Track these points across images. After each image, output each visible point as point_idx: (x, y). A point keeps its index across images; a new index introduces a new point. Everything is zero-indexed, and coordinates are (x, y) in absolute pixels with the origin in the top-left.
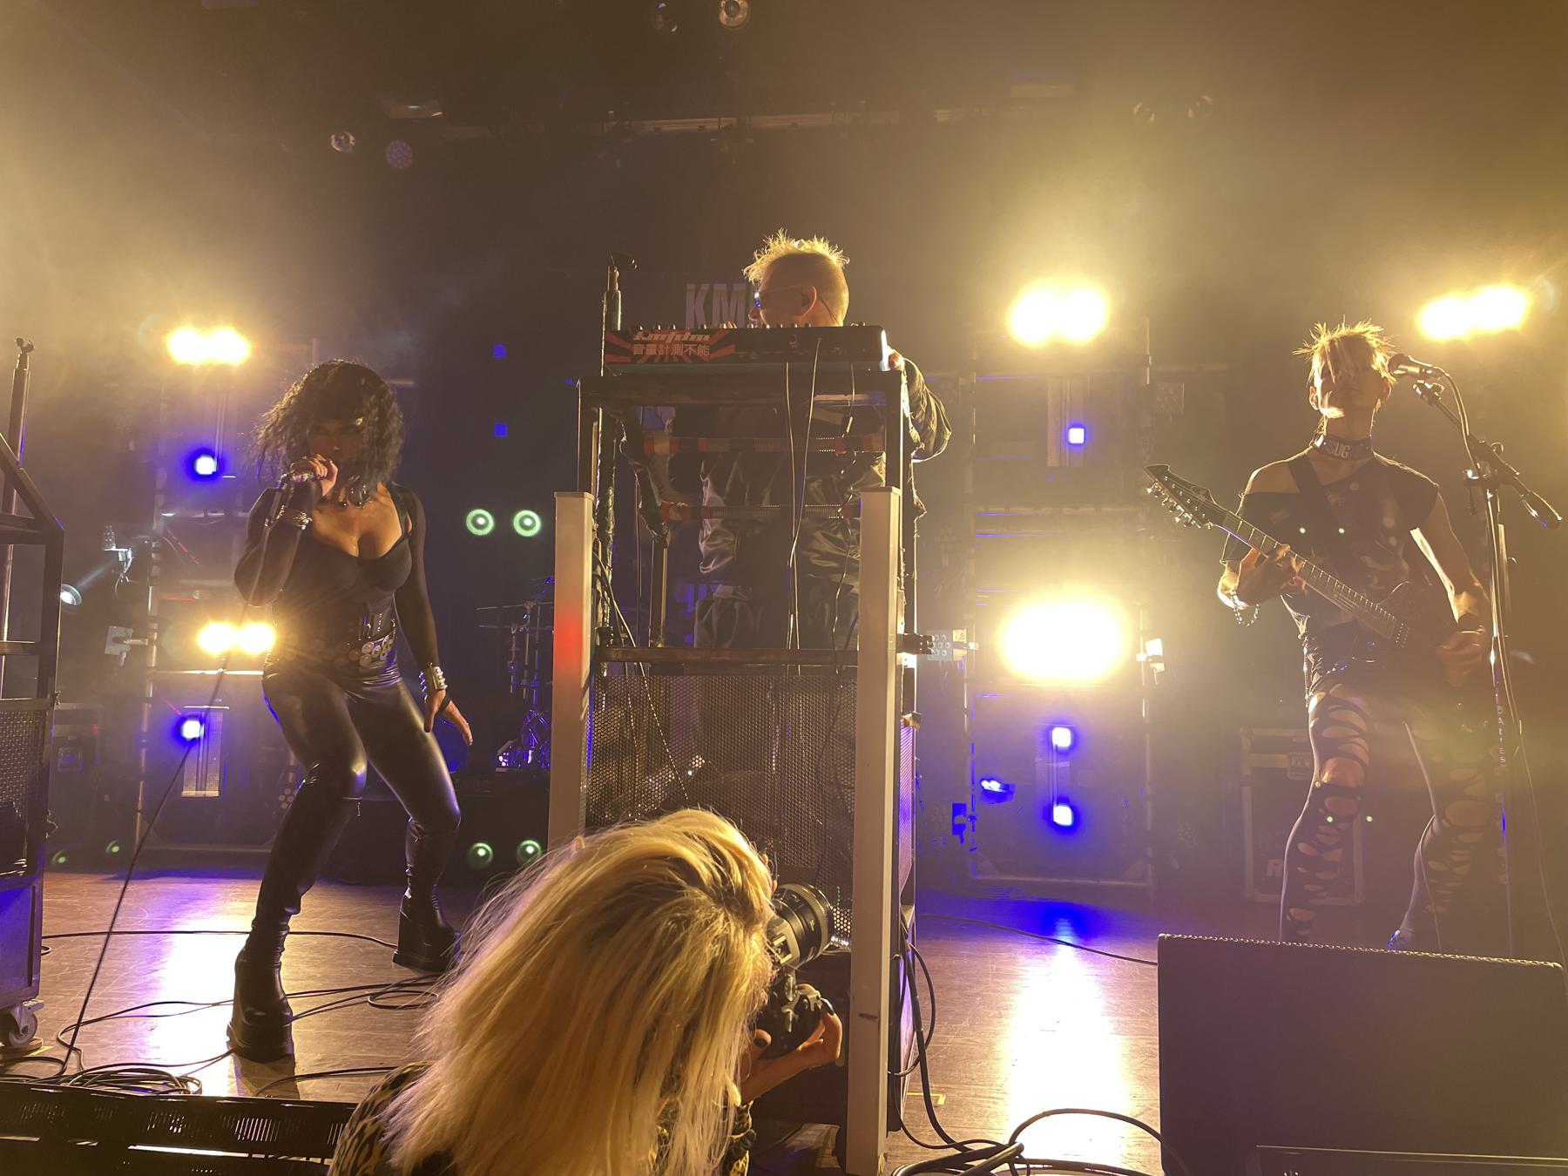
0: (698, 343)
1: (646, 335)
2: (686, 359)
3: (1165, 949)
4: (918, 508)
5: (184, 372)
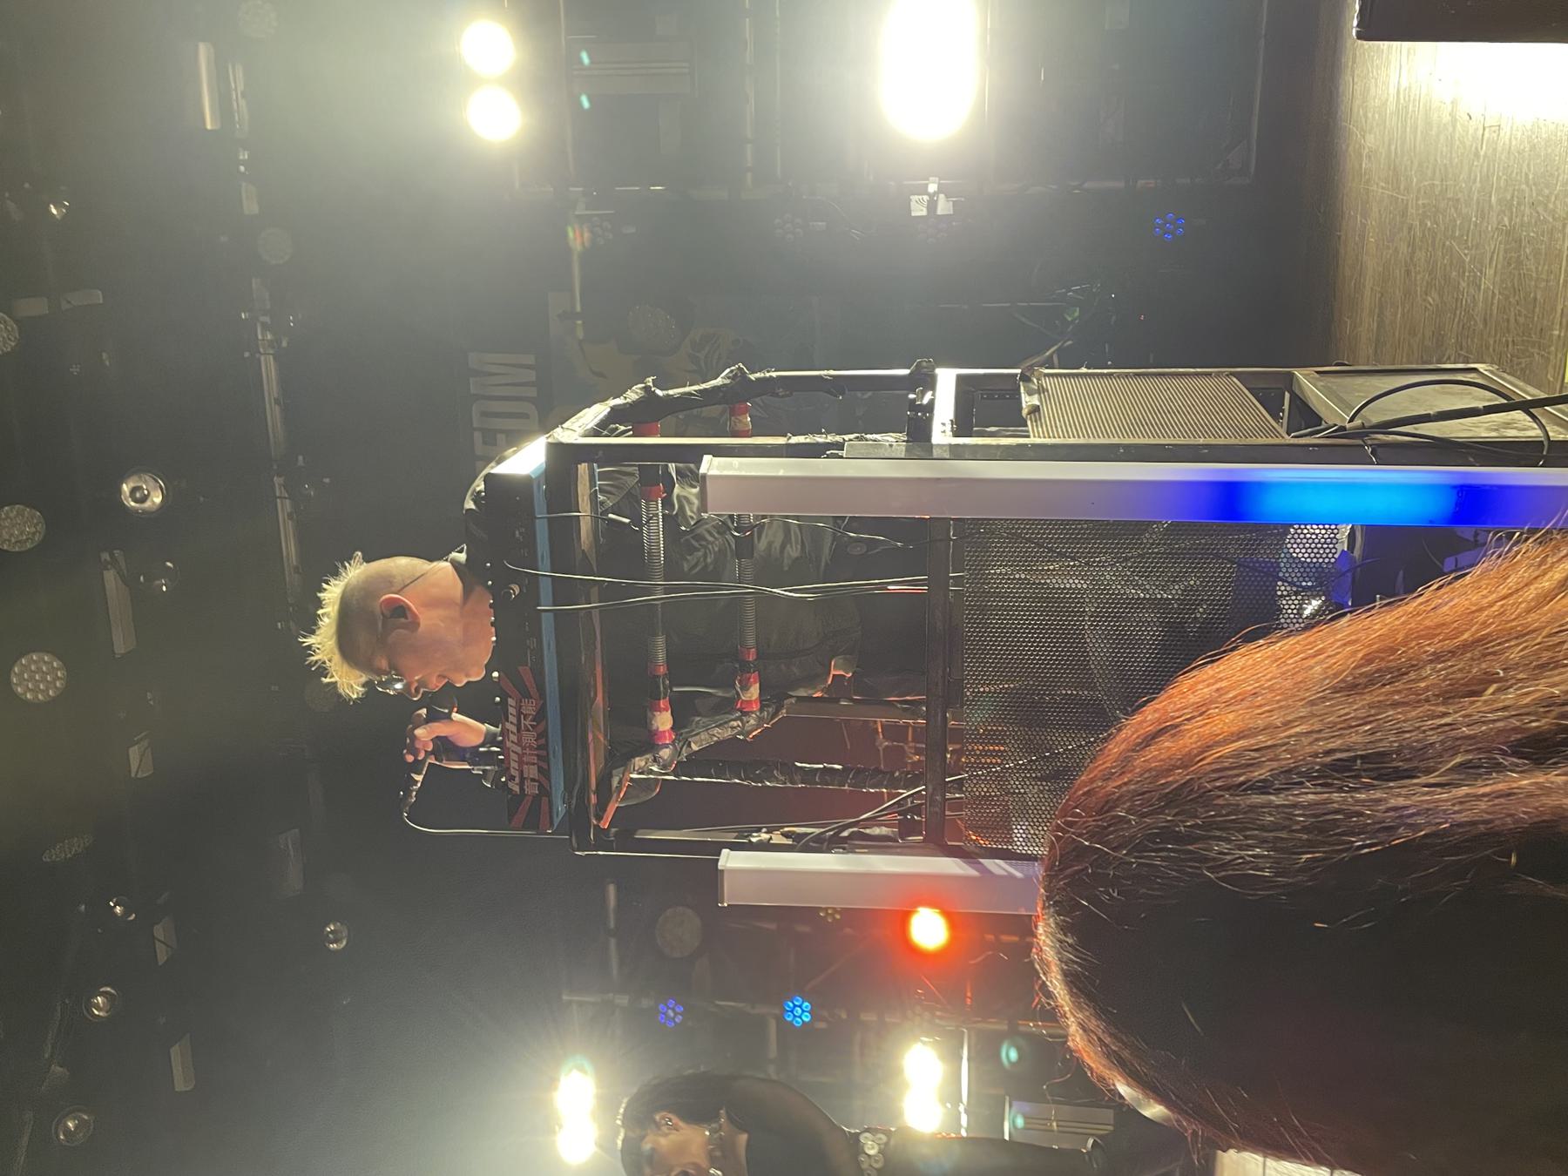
0: (519, 713)
1: (512, 778)
2: (541, 728)
3: (1371, 31)
4: (734, 378)
5: (605, 1145)
